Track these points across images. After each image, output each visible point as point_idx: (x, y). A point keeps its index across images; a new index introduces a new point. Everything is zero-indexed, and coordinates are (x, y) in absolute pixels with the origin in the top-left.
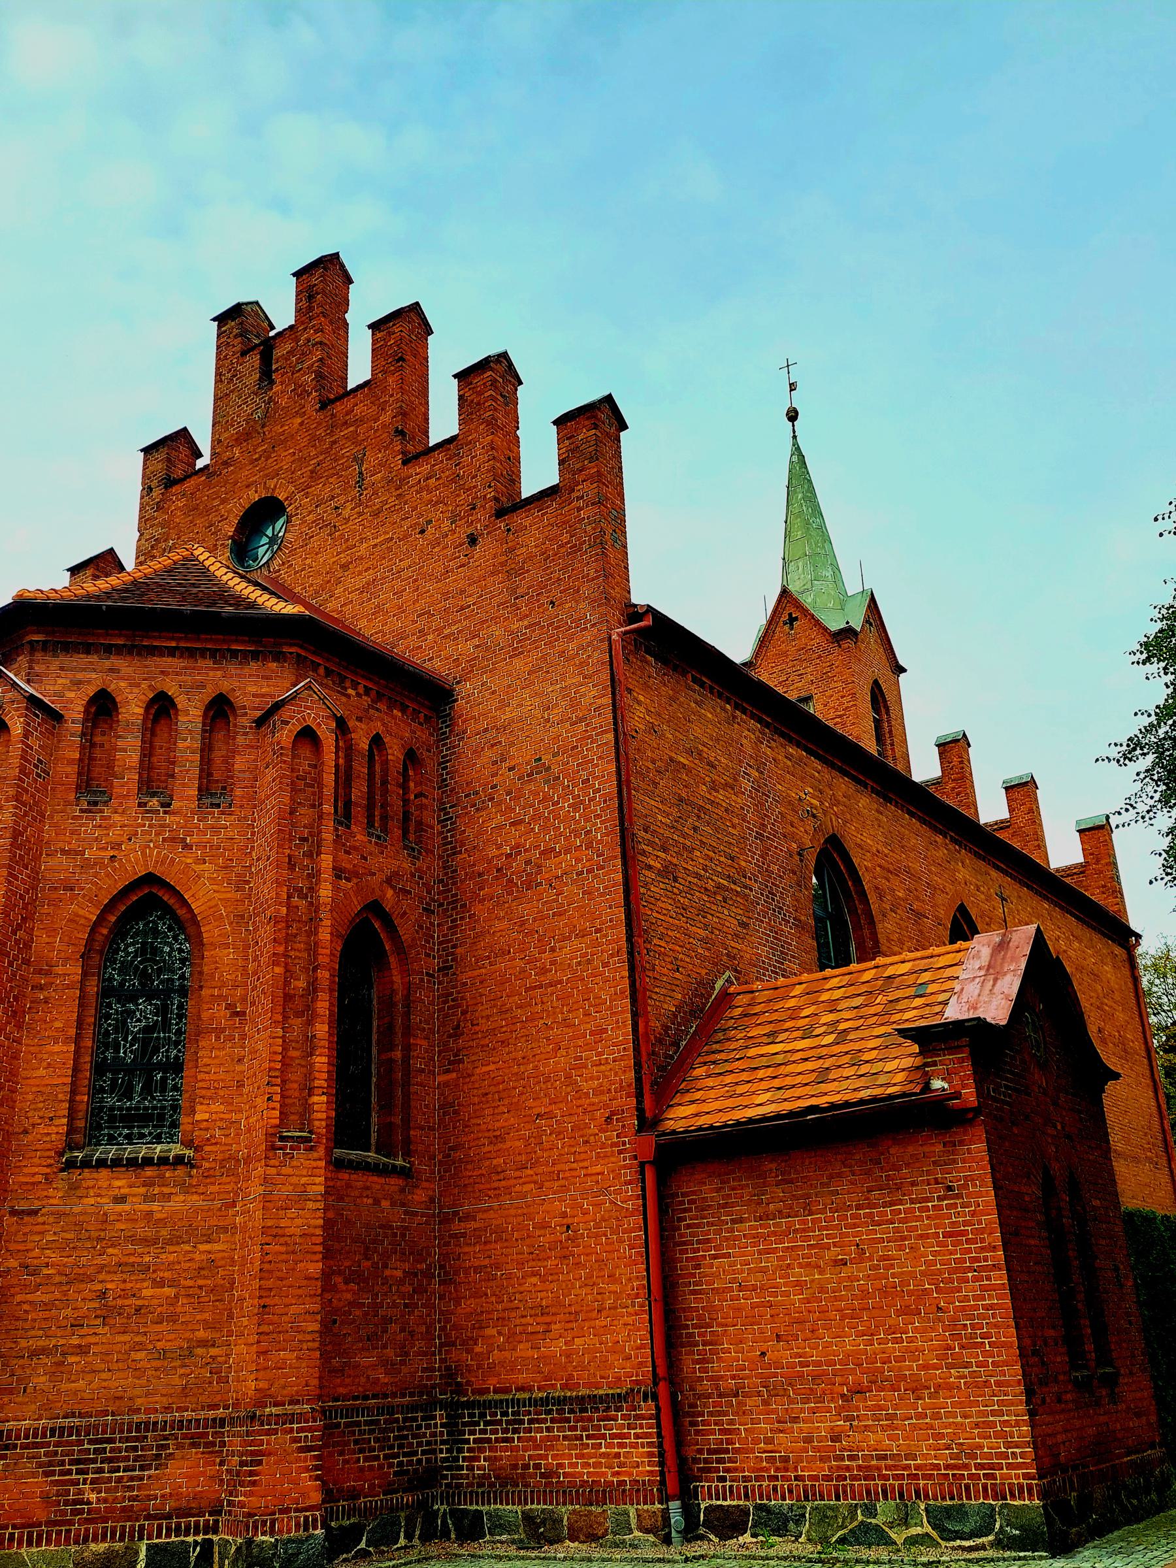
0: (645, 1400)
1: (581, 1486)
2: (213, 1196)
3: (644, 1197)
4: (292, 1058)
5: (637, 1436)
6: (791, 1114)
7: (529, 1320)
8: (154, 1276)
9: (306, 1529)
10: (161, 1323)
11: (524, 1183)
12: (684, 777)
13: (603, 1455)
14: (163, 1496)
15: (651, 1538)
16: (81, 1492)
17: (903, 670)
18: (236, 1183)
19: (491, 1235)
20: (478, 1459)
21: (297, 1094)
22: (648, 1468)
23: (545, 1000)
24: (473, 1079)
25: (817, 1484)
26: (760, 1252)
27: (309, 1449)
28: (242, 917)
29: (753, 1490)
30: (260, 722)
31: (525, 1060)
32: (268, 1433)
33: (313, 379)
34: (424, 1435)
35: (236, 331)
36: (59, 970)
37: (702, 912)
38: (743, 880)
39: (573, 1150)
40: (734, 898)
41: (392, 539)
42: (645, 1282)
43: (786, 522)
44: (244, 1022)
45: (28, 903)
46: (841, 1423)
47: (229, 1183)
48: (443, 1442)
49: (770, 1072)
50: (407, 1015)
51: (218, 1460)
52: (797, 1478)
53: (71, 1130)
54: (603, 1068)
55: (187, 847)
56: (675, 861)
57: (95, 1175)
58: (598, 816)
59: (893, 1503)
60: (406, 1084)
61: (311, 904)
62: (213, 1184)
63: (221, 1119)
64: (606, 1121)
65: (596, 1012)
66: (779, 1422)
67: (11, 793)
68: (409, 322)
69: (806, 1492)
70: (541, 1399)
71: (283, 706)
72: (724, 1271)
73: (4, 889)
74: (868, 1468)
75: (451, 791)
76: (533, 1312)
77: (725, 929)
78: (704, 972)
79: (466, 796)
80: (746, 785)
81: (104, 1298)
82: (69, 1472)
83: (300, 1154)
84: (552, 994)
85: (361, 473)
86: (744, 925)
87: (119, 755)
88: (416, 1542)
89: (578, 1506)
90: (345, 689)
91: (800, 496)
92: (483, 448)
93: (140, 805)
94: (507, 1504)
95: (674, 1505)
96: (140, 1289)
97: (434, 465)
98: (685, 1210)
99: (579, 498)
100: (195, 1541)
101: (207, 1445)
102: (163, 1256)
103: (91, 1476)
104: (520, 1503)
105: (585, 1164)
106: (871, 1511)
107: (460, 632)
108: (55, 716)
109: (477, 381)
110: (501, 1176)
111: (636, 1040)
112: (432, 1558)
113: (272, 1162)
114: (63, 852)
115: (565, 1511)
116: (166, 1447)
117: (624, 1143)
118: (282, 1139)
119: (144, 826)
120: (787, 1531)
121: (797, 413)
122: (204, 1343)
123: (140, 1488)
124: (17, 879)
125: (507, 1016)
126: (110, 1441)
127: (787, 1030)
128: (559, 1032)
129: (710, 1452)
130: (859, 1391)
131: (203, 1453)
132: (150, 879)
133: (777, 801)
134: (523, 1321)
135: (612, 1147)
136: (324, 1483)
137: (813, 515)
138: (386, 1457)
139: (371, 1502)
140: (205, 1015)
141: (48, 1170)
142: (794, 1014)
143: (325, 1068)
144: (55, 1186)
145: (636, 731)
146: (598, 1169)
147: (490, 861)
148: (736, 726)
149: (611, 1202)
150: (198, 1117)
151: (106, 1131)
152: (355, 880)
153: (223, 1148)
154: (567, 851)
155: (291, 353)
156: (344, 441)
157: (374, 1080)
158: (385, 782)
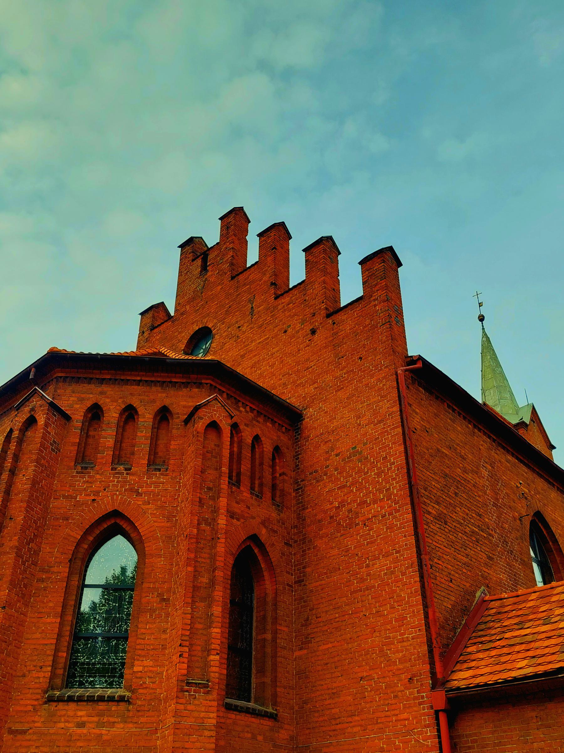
2: (142, 725)
3: (439, 737)
4: (197, 629)
6: (546, 674)
12: (447, 461)
17: (554, 448)
18: (158, 716)
21: (200, 654)
23: (364, 598)
24: (317, 653)
28: (170, 538)
30: (187, 421)
31: (352, 640)
33: (228, 266)
35: (190, 251)
36: (55, 569)
37: (465, 546)
38: (487, 530)
39: (387, 702)
40: (483, 540)
41: (268, 338)
43: (482, 371)
44: (168, 605)
45: (39, 527)
47: (153, 716)
49: (523, 647)
50: (275, 610)
54: (405, 644)
55: (139, 494)
56: (445, 511)
57: (66, 707)
58: (394, 479)
60: (274, 656)
61: (213, 529)
62: (143, 716)
63: (151, 671)
64: (409, 681)
65: (399, 606)
67: (34, 458)
68: (279, 231)
71: (199, 408)
73: (24, 515)
75: (301, 472)
77: (479, 559)
78: (468, 585)
79: (310, 474)
80: (485, 473)
83: (200, 696)
84: (368, 595)
85: (252, 308)
86: (490, 558)
90: (239, 407)
91: (489, 357)
92: (319, 284)
93: (112, 469)
97: (292, 297)
99: (374, 300)
105: (397, 712)
107: (306, 381)
108: (67, 418)
109: (315, 250)
110: (338, 721)
111: (427, 625)
113: (181, 701)
117: (423, 697)
118: (188, 684)
119: (114, 481)
121: (484, 317)
124: (33, 510)
125: (339, 611)
127: (531, 620)
128: (373, 621)
132: (116, 514)
133: (504, 486)
135: (414, 700)
137: (496, 366)
140: (144, 600)
142: (535, 610)
143: (219, 636)
144: (39, 714)
145: (416, 429)
146: (405, 715)
147: (325, 512)
148: (475, 438)
149: (416, 740)
150: (135, 669)
152: (242, 520)
153: (151, 691)
154: (375, 502)
155: (217, 256)
156: (244, 294)
157: (254, 653)
158: (261, 464)
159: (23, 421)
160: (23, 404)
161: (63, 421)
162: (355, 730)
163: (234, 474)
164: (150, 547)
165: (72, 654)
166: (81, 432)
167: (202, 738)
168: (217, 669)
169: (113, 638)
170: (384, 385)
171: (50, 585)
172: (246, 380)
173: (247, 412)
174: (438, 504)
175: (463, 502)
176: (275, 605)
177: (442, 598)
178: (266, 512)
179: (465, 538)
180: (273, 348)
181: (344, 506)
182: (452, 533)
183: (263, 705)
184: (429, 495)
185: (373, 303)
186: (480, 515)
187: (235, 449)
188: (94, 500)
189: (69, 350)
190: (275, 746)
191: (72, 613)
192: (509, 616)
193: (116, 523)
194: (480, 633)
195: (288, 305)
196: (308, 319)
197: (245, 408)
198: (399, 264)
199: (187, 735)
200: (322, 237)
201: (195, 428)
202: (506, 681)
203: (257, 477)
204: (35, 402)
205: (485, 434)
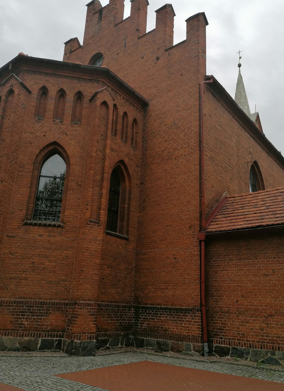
0: (198, 311)
1: (175, 335)
5: (194, 322)
6: (252, 227)
7: (162, 284)
8: (49, 259)
9: (90, 339)
10: (51, 273)
11: (162, 245)
12: (218, 132)
13: (183, 327)
14: (47, 325)
15: (198, 353)
16: (22, 321)
19: (151, 259)
20: (144, 324)
22: (198, 332)
23: (172, 192)
25: (254, 343)
26: (238, 270)
27: (93, 315)
28: (82, 157)
29: (232, 343)
30: (91, 100)
32: (80, 309)
34: (128, 315)
36: (26, 167)
39: (178, 236)
41: (133, 61)
42: (199, 276)
45: (18, 146)
46: (264, 325)
48: (133, 318)
50: (130, 195)
51: (65, 316)
52: (247, 341)
53: (27, 214)
54: (189, 212)
56: (214, 156)
57: (34, 228)
58: (192, 138)
59: (281, 352)
63: (73, 215)
64: (189, 228)
65: (188, 196)
66: (242, 323)
69: (250, 345)
70: (164, 308)
72: (225, 275)
74: (273, 340)
76: (163, 283)
77: (227, 179)
78: (220, 190)
81: (34, 264)
82: (19, 315)
84: (174, 191)
86: (231, 179)
87: (48, 106)
88: (124, 346)
89: (174, 341)
90: (117, 96)
93: (53, 121)
94: (152, 338)
95: (206, 344)
96: (45, 263)
97: (147, 38)
98: (213, 256)
100: (56, 339)
101: (62, 311)
102: (52, 253)
103: (25, 317)
104: (156, 338)
105: (182, 240)
106: (273, 354)
108: (30, 92)
112: (128, 352)
113: (87, 228)
114: (29, 132)
115: (170, 342)
116: (49, 310)
117: (195, 235)
118: (90, 221)
120: (243, 357)
121: (241, 65)
122: (63, 280)
123: (40, 322)
126: (33, 307)
127: (248, 206)
129: (217, 329)
130: (271, 315)
131: (61, 313)
132: (55, 143)
134: (160, 285)
136: (97, 326)
138: (116, 320)
139: (111, 333)
140: (69, 185)
141: (19, 225)
143: (105, 203)
144: (21, 230)
146: (186, 242)
149: (190, 252)
151: (38, 216)
154: (181, 149)
157: (119, 213)
158: (127, 127)
159: (7, 91)
160: (6, 82)
161: (28, 94)
162: (163, 246)
163: (114, 130)
164: (72, 160)
165: (35, 206)
166: (37, 100)
167: (96, 244)
168: (103, 217)
169: (54, 200)
170: (192, 90)
171: (24, 174)
172: (122, 82)
173: (121, 99)
174: (212, 151)
175: (223, 152)
176: (130, 192)
177: (208, 194)
178: (128, 150)
179: (222, 169)
180: (136, 67)
181: (166, 150)
182: (216, 166)
183: (122, 234)
184: (208, 147)
185: (191, 44)
186: (229, 159)
187: (115, 118)
188: (44, 135)
189: (30, 55)
190: (127, 251)
191: (35, 187)
192: (237, 204)
193: (55, 148)
194: (223, 211)
195: (145, 42)
196: (155, 51)
197: (120, 97)
198: (207, 23)
199: (89, 242)
200: (167, 4)
201: (95, 104)
202: (234, 230)
203: (125, 133)
204: (12, 81)
205: (237, 121)
